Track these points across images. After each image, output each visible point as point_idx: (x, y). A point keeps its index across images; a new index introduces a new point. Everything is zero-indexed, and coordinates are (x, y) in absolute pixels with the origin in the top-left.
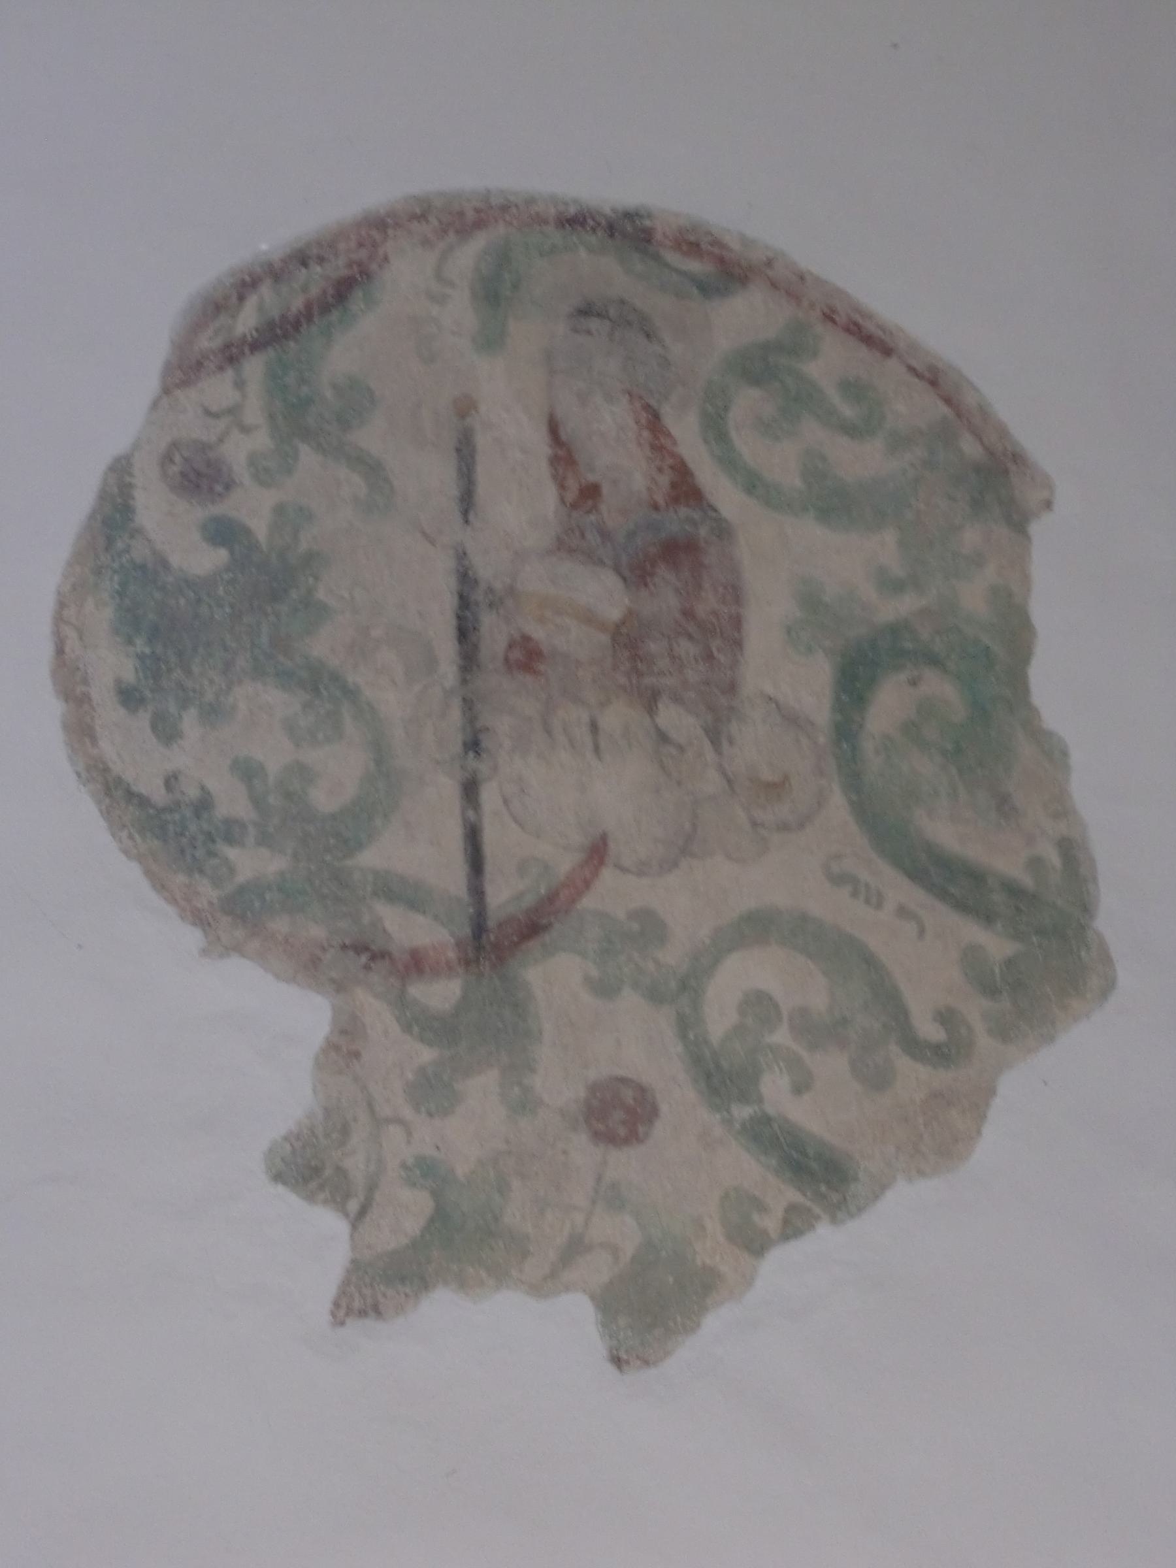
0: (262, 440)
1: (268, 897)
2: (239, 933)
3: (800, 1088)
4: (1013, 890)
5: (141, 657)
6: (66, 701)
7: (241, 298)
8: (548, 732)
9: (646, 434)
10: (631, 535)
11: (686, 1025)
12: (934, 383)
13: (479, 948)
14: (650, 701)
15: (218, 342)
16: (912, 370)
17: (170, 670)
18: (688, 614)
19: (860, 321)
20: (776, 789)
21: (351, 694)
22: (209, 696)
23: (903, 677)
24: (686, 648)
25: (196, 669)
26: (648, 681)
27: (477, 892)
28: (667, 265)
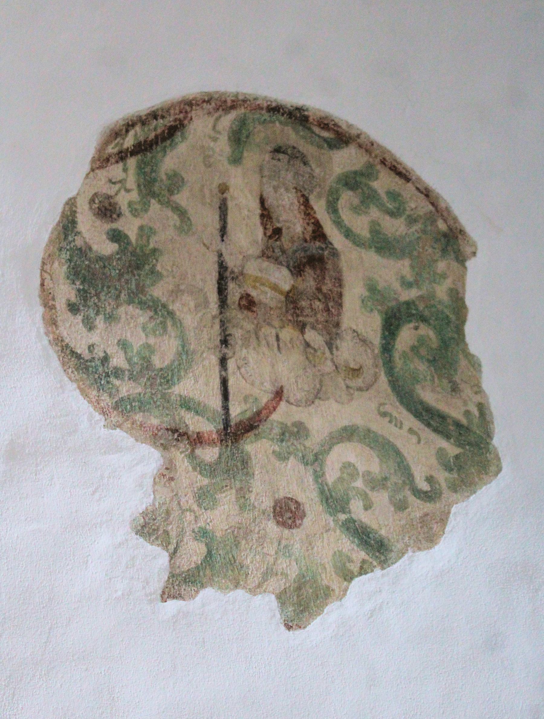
0: (134, 196)
1: (133, 404)
2: (121, 419)
3: (367, 508)
4: (458, 425)
5: (79, 290)
6: (45, 307)
7: (127, 131)
8: (258, 338)
9: (302, 207)
10: (295, 252)
11: (319, 476)
12: (427, 196)
13: (226, 435)
14: (302, 327)
15: (116, 150)
16: (418, 189)
17: (91, 297)
18: (319, 290)
19: (396, 165)
20: (356, 372)
21: (171, 314)
22: (108, 310)
23: (412, 325)
24: (318, 305)
25: (103, 298)
26: (301, 319)
27: (226, 408)
28: (313, 132)
